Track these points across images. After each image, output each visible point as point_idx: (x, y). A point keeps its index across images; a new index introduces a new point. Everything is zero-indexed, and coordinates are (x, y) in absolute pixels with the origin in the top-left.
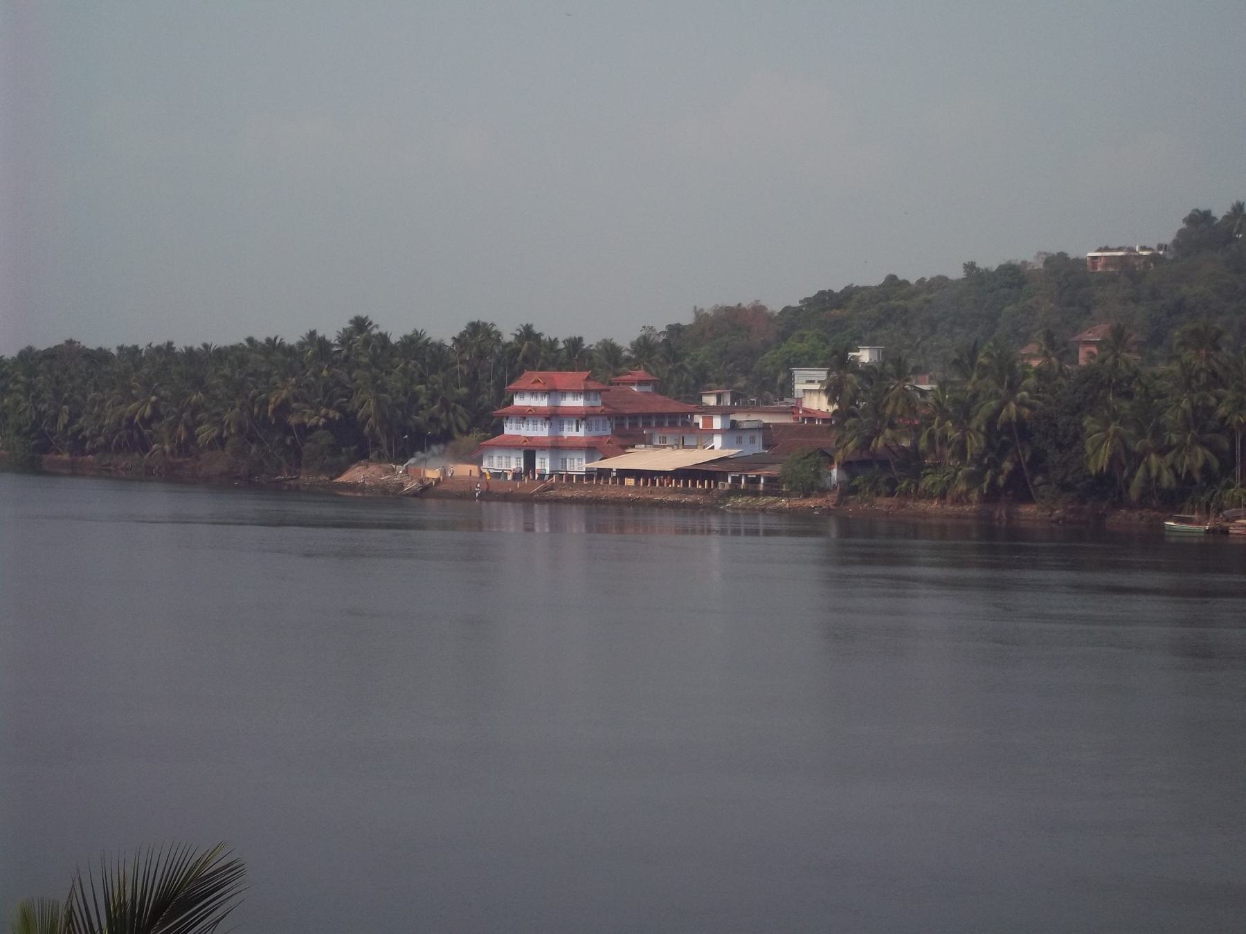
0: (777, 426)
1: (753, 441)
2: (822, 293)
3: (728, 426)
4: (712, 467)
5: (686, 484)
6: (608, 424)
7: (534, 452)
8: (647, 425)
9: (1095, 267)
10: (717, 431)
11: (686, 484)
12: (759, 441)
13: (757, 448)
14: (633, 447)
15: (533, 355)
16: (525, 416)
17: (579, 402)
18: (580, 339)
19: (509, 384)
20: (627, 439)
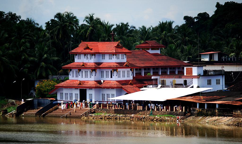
0: (236, 73)
1: (218, 82)
2: (185, 16)
3: (202, 74)
4: (189, 99)
5: (172, 109)
6: (131, 73)
7: (86, 90)
8: (156, 74)
9: (20, 116)
10: (195, 77)
11: (172, 109)
12: (222, 80)
13: (221, 86)
14: (146, 87)
15: (97, 31)
16: (81, 68)
17: (114, 60)
18: (218, 3)
19: (73, 49)
20: (141, 82)
